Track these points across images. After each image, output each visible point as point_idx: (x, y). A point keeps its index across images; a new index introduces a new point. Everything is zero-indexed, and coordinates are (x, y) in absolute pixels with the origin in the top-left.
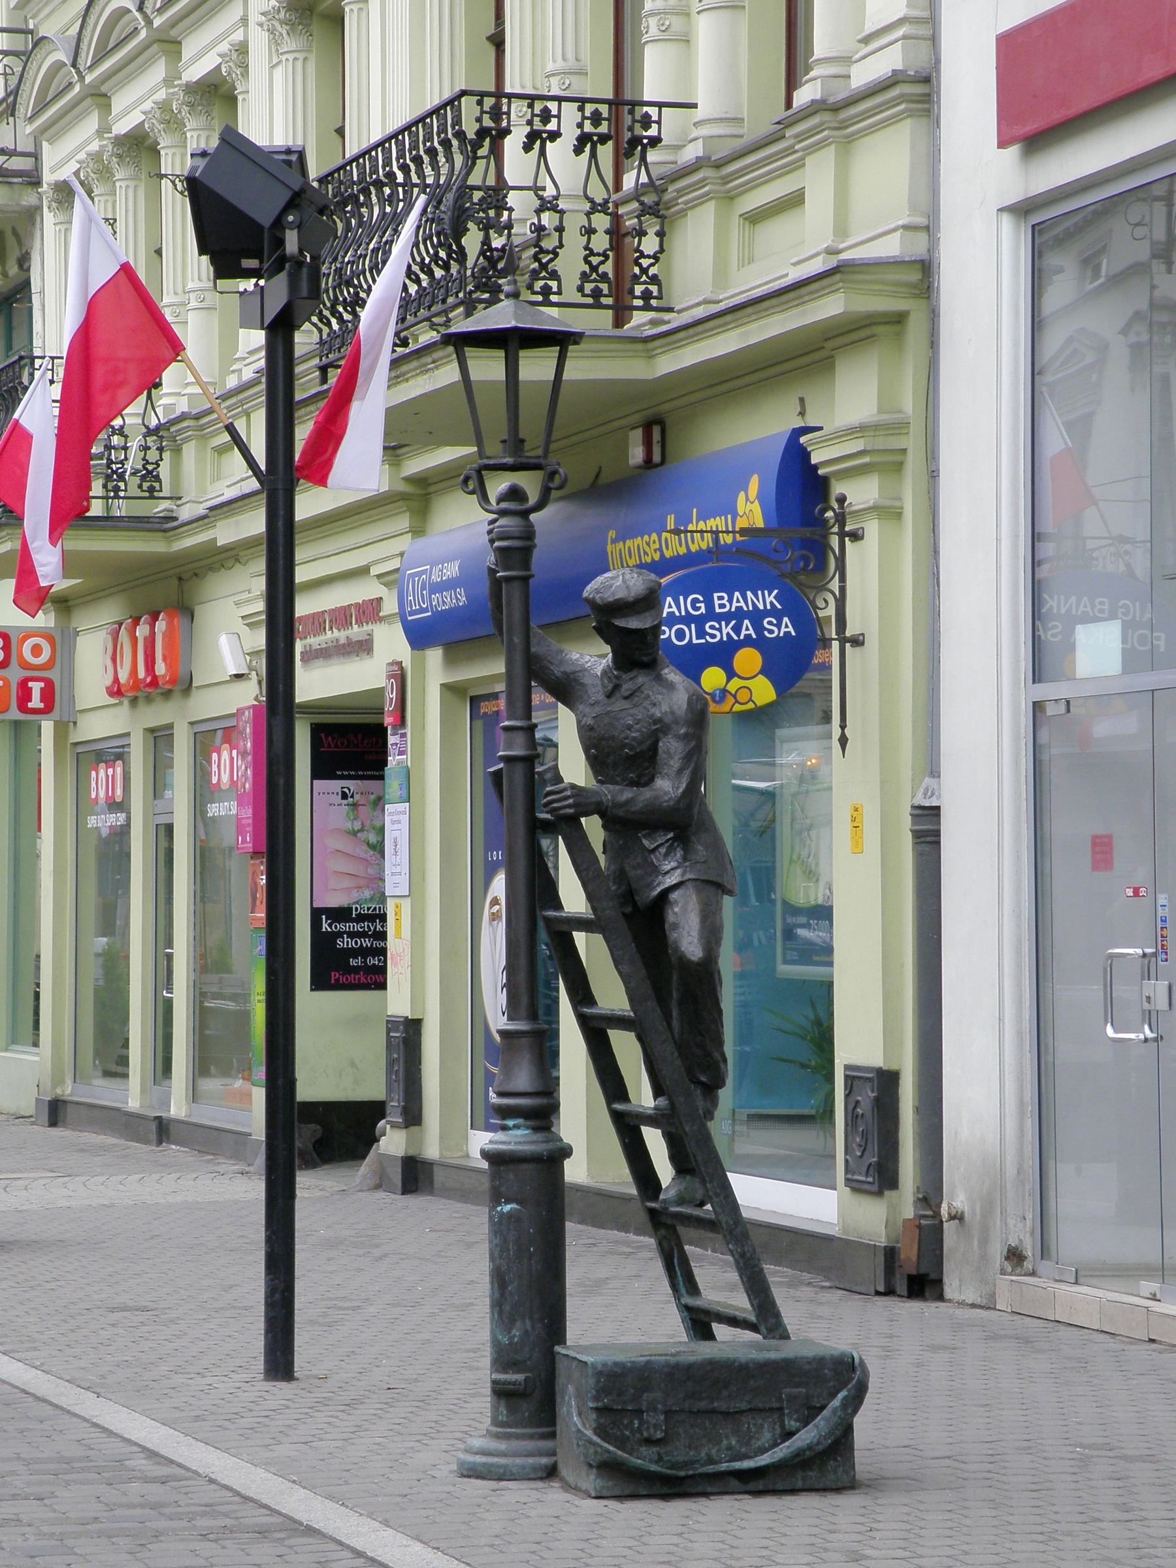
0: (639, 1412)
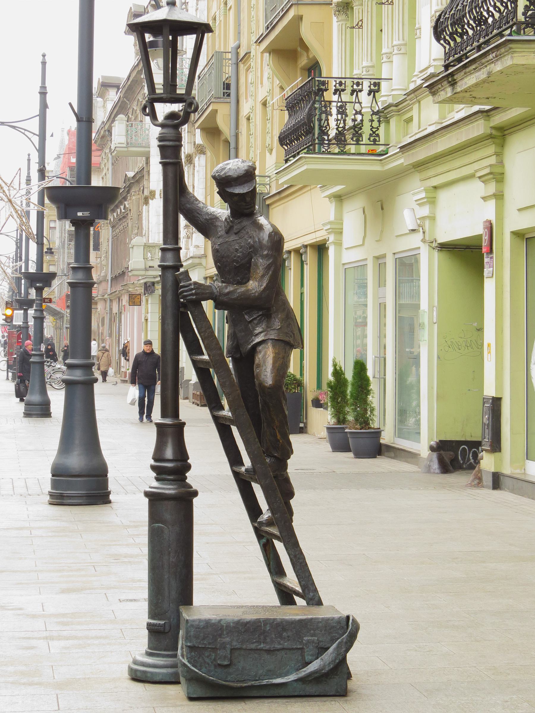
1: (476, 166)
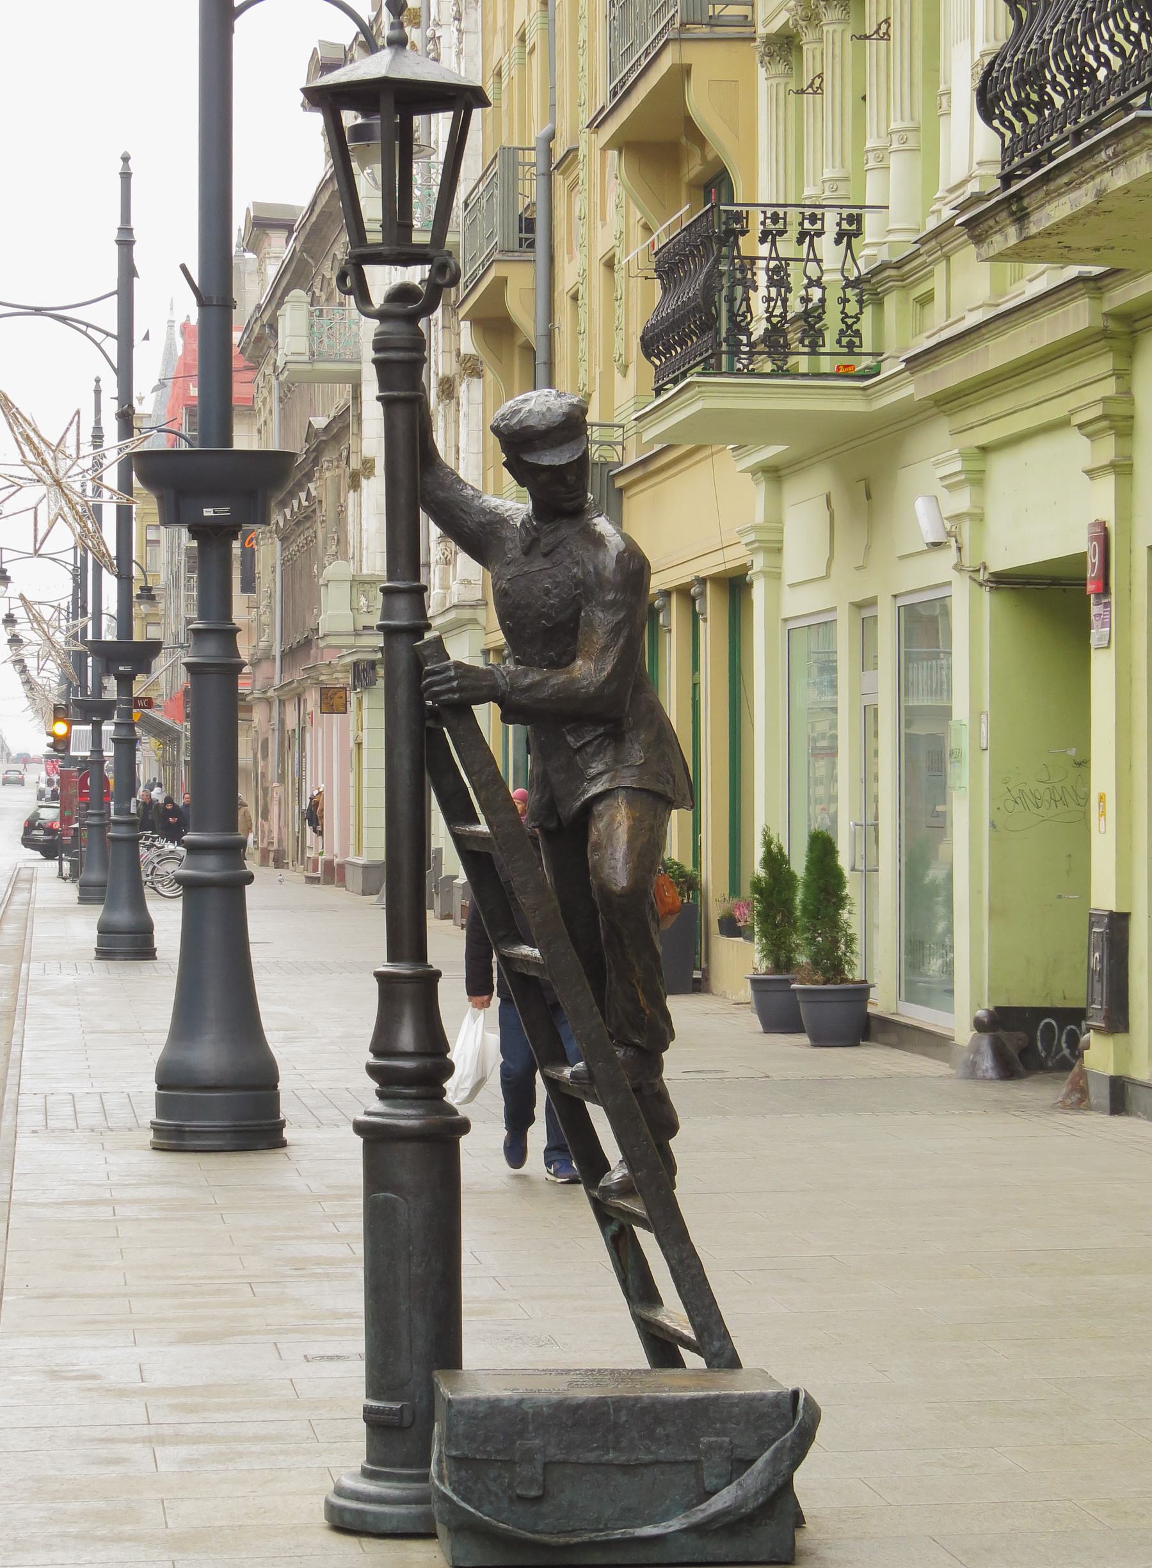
0: (509, 1464)
1: (1072, 401)
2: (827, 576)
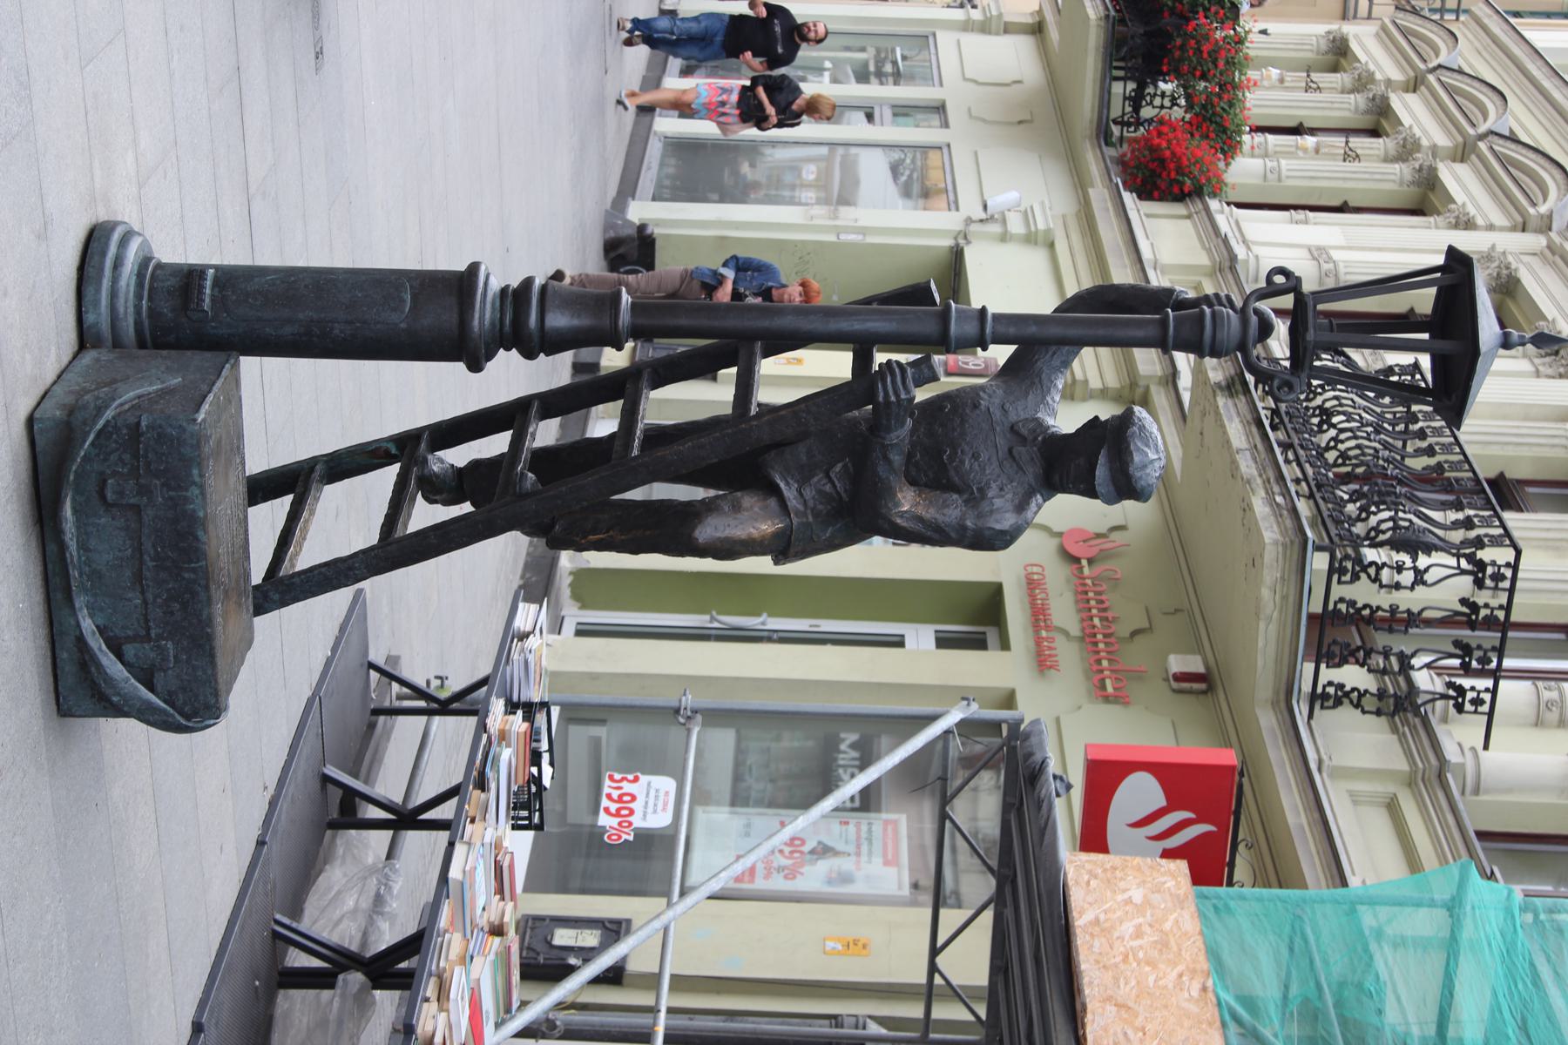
2: (965, 79)
